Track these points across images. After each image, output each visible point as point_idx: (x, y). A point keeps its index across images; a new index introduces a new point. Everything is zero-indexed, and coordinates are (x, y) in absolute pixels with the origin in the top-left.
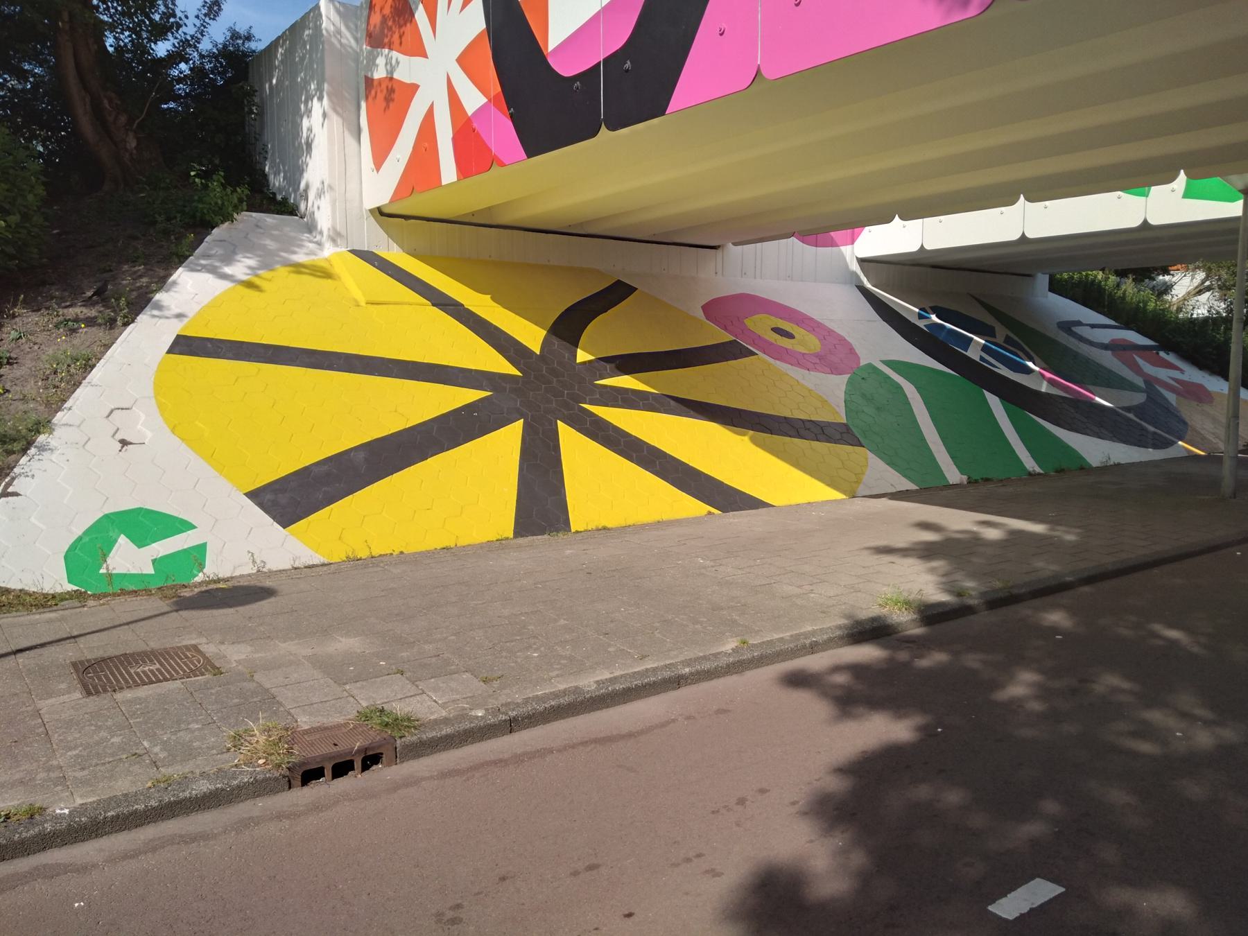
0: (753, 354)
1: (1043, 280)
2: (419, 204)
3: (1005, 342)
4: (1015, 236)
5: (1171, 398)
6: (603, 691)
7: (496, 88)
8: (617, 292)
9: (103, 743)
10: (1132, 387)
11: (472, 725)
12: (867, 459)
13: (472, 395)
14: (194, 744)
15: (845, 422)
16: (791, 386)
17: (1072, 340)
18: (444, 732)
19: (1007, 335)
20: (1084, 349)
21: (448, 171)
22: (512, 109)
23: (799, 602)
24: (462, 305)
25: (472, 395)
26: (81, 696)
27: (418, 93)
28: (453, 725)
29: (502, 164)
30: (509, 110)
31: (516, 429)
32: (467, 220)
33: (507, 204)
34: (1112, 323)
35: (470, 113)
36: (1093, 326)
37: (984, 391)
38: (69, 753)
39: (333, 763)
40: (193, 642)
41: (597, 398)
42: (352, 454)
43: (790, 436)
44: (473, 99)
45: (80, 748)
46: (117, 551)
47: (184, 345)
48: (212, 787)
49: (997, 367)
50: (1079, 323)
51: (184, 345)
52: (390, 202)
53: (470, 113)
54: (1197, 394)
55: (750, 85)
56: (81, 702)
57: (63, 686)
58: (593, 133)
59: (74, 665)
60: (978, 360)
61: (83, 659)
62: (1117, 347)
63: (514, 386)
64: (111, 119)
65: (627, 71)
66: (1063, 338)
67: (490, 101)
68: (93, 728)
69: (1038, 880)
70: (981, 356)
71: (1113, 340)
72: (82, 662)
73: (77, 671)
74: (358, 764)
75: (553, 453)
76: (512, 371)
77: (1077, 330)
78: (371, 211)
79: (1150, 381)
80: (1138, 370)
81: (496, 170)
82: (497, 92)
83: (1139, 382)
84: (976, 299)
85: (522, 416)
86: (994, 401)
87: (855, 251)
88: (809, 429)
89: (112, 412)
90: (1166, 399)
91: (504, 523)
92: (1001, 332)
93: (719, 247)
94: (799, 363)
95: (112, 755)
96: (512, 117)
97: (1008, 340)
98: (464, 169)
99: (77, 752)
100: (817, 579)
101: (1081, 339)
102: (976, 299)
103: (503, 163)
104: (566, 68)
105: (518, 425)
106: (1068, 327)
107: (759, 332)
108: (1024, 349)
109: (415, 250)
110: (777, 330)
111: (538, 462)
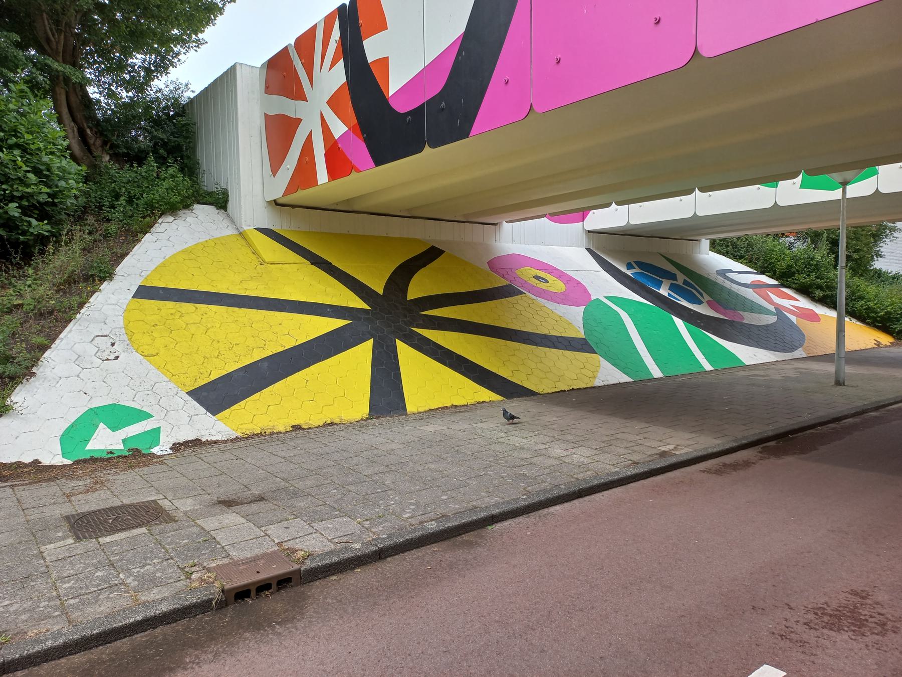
0: (523, 293)
1: (705, 243)
2: (303, 195)
3: (683, 284)
4: (689, 215)
5: (793, 318)
6: (441, 528)
7: (354, 121)
8: (432, 254)
9: (89, 577)
10: (767, 312)
11: (352, 555)
12: (599, 361)
13: (339, 323)
14: (157, 575)
15: (584, 337)
16: (548, 314)
17: (726, 281)
18: (333, 560)
19: (677, 281)
20: (735, 288)
21: (322, 176)
22: (365, 135)
23: (566, 460)
24: (331, 263)
25: (339, 323)
26: (73, 542)
27: (302, 122)
28: (339, 555)
29: (358, 171)
30: (363, 135)
31: (369, 345)
32: (333, 208)
33: (361, 197)
34: (753, 270)
35: (336, 137)
36: (740, 273)
37: (673, 316)
38: (64, 586)
39: (256, 587)
40: (153, 498)
41: (421, 324)
42: (260, 364)
43: (549, 347)
44: (339, 129)
45: (73, 582)
46: (98, 435)
47: (145, 292)
48: (171, 608)
49: (679, 300)
50: (731, 271)
51: (145, 292)
52: (282, 196)
53: (336, 137)
54: (814, 317)
55: (527, 115)
56: (74, 545)
57: (60, 534)
58: (419, 150)
59: (67, 518)
60: (667, 296)
61: (74, 513)
62: (754, 286)
63: (366, 316)
64: (91, 141)
65: (443, 109)
66: (720, 280)
67: (350, 129)
68: (82, 565)
69: (765, 667)
70: (669, 293)
71: (752, 282)
72: (73, 516)
73: (69, 522)
74: (274, 586)
75: (394, 361)
76: (365, 306)
77: (730, 275)
78: (269, 202)
79: (779, 308)
80: (771, 302)
81: (354, 174)
82: (355, 123)
83: (772, 308)
84: (661, 255)
85: (372, 336)
86: (679, 322)
87: (585, 228)
88: (561, 342)
89: (94, 339)
90: (789, 319)
91: (362, 409)
92: (681, 278)
93: (497, 223)
94: (552, 299)
95: (97, 586)
96: (365, 140)
97: (685, 282)
98: (333, 174)
99: (70, 585)
100: (577, 444)
101: (733, 281)
102: (661, 255)
103: (358, 169)
104: (402, 107)
105: (371, 341)
106: (723, 273)
107: (526, 279)
108: (696, 288)
109: (348, 231)
110: (537, 278)
111: (384, 367)
